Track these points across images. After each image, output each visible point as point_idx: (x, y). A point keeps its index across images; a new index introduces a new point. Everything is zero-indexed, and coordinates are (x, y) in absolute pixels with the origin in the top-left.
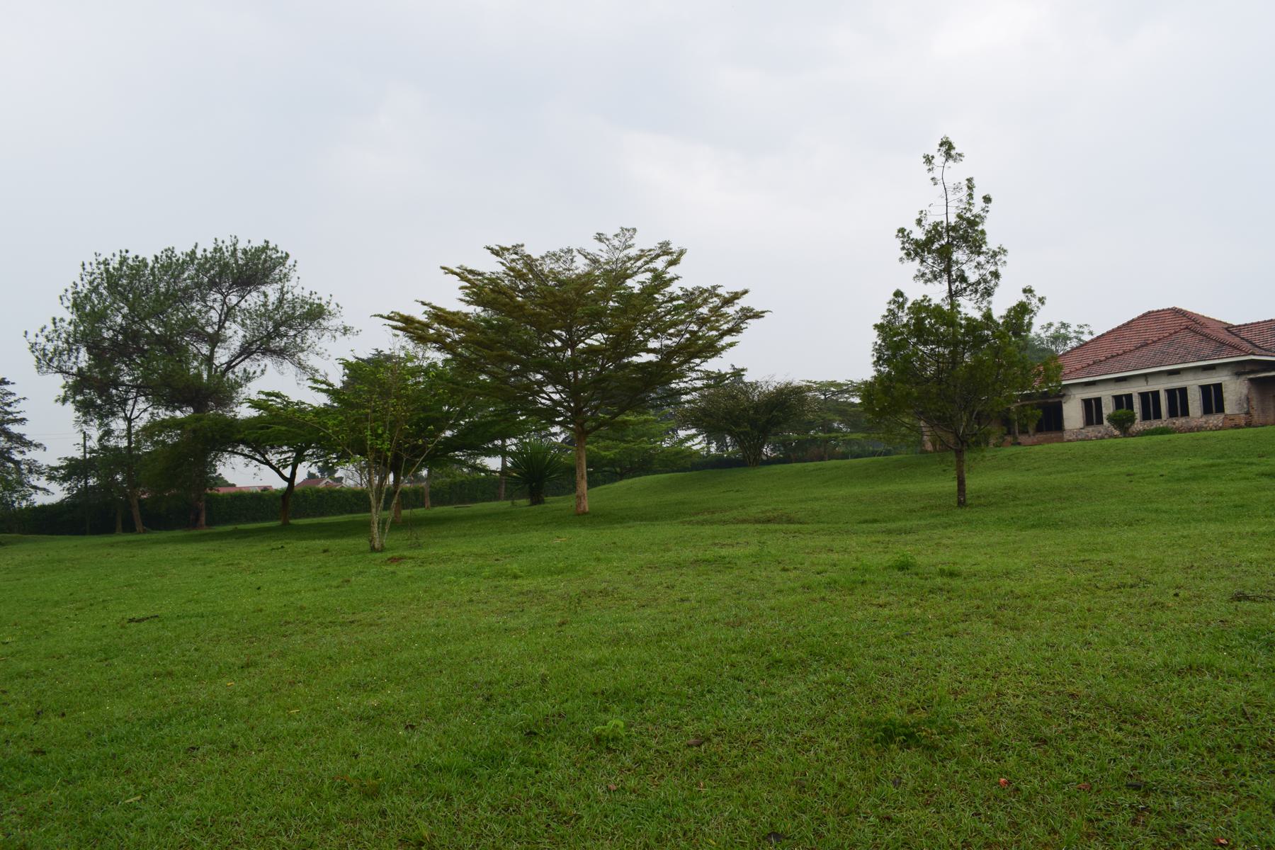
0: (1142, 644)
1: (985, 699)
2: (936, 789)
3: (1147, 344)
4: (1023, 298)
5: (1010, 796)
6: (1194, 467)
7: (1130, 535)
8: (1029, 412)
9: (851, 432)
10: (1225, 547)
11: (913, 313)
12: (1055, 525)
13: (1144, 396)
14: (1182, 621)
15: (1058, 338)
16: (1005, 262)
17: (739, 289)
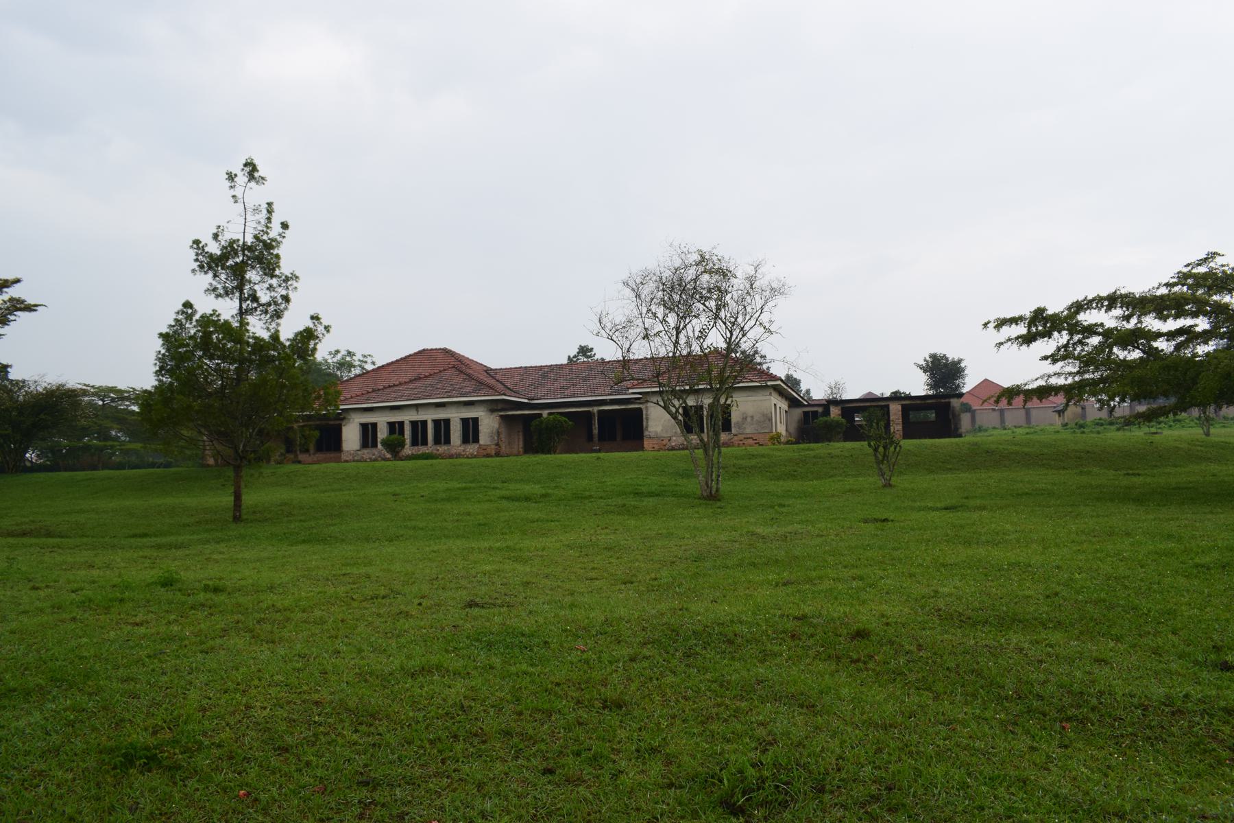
0: (385, 650)
1: (233, 713)
2: (174, 810)
3: (420, 378)
4: (310, 324)
5: (248, 807)
6: (450, 490)
7: (389, 550)
8: (308, 432)
9: (129, 442)
10: (466, 560)
11: (200, 326)
12: (323, 540)
13: (414, 424)
14: (422, 628)
15: (344, 365)
16: (296, 288)
17: (11, 277)
